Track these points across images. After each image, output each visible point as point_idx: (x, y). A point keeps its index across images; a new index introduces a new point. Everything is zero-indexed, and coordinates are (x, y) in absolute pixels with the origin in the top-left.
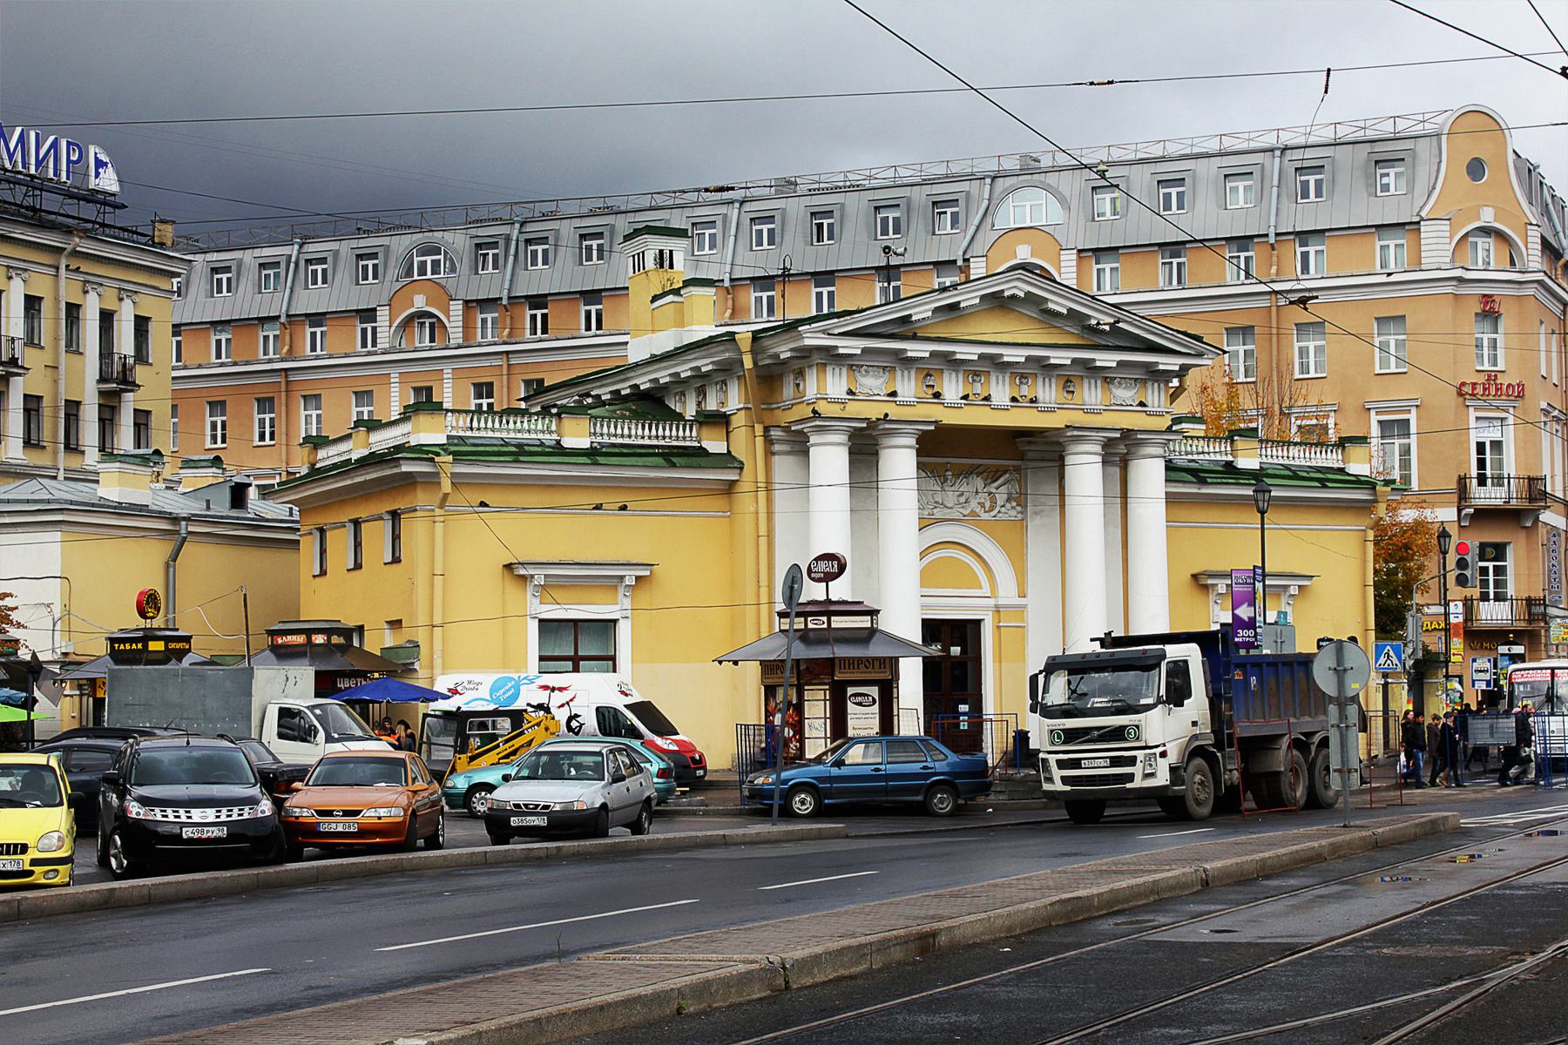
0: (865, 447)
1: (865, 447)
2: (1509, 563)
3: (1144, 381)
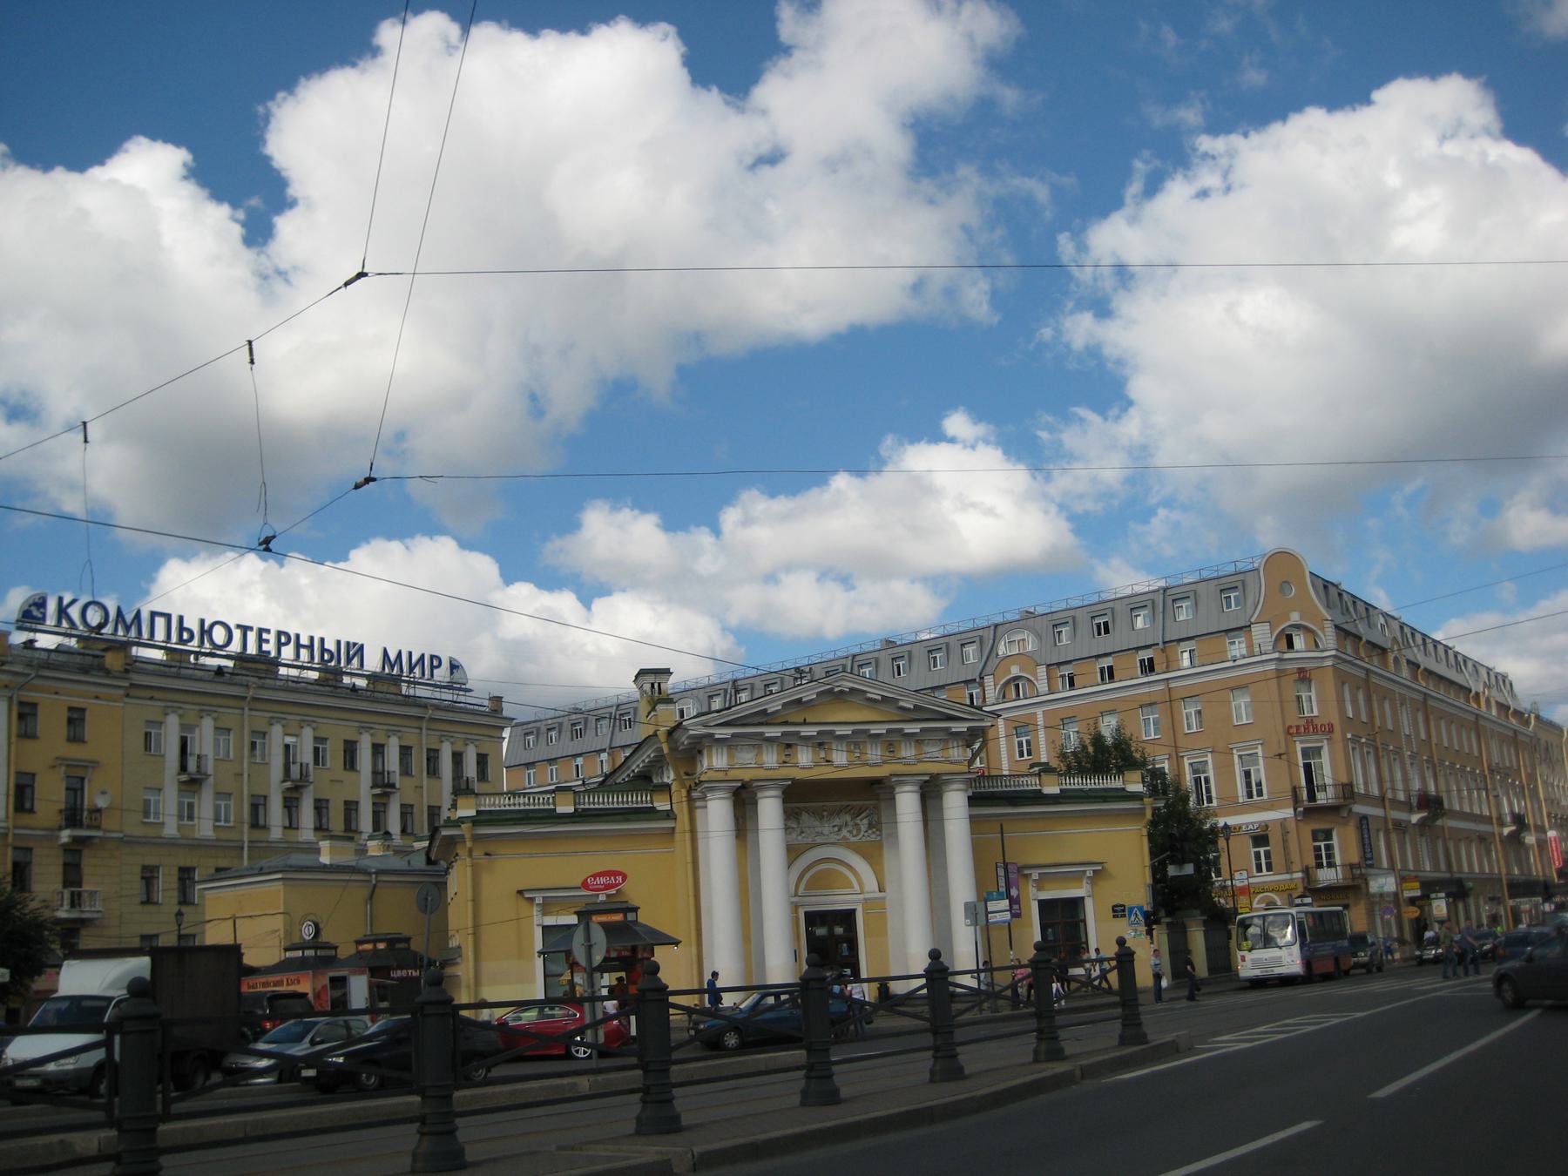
0: (744, 799)
1: (931, 792)
2: (1335, 842)
3: (946, 741)
